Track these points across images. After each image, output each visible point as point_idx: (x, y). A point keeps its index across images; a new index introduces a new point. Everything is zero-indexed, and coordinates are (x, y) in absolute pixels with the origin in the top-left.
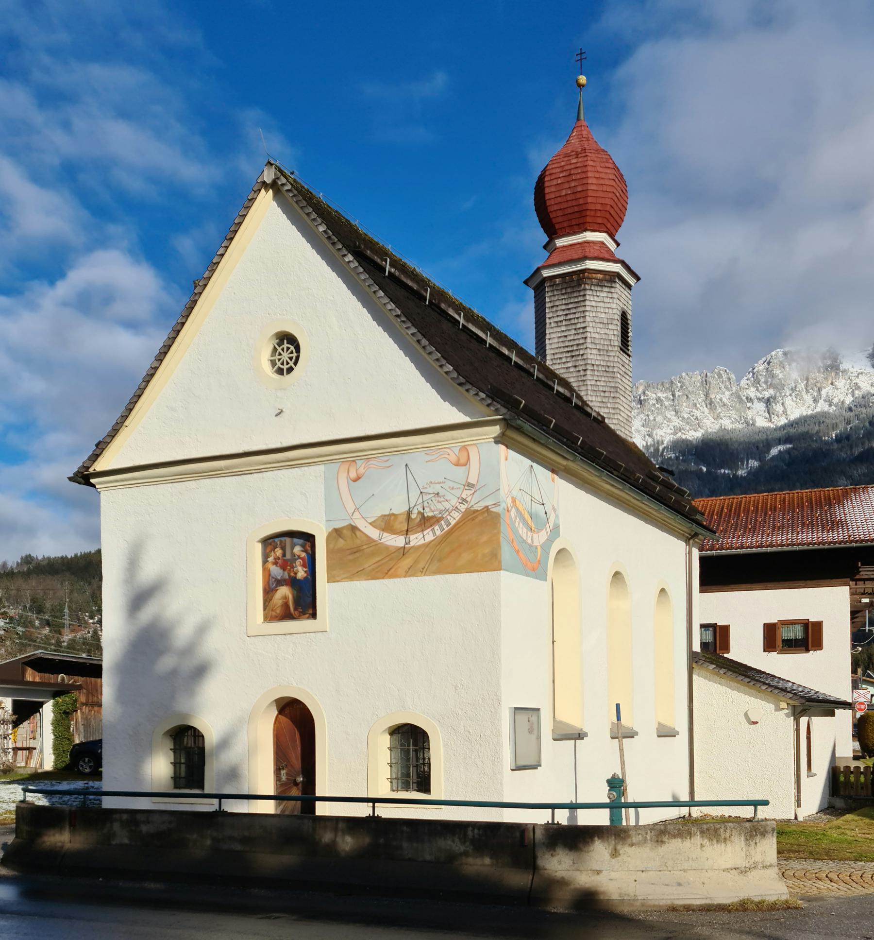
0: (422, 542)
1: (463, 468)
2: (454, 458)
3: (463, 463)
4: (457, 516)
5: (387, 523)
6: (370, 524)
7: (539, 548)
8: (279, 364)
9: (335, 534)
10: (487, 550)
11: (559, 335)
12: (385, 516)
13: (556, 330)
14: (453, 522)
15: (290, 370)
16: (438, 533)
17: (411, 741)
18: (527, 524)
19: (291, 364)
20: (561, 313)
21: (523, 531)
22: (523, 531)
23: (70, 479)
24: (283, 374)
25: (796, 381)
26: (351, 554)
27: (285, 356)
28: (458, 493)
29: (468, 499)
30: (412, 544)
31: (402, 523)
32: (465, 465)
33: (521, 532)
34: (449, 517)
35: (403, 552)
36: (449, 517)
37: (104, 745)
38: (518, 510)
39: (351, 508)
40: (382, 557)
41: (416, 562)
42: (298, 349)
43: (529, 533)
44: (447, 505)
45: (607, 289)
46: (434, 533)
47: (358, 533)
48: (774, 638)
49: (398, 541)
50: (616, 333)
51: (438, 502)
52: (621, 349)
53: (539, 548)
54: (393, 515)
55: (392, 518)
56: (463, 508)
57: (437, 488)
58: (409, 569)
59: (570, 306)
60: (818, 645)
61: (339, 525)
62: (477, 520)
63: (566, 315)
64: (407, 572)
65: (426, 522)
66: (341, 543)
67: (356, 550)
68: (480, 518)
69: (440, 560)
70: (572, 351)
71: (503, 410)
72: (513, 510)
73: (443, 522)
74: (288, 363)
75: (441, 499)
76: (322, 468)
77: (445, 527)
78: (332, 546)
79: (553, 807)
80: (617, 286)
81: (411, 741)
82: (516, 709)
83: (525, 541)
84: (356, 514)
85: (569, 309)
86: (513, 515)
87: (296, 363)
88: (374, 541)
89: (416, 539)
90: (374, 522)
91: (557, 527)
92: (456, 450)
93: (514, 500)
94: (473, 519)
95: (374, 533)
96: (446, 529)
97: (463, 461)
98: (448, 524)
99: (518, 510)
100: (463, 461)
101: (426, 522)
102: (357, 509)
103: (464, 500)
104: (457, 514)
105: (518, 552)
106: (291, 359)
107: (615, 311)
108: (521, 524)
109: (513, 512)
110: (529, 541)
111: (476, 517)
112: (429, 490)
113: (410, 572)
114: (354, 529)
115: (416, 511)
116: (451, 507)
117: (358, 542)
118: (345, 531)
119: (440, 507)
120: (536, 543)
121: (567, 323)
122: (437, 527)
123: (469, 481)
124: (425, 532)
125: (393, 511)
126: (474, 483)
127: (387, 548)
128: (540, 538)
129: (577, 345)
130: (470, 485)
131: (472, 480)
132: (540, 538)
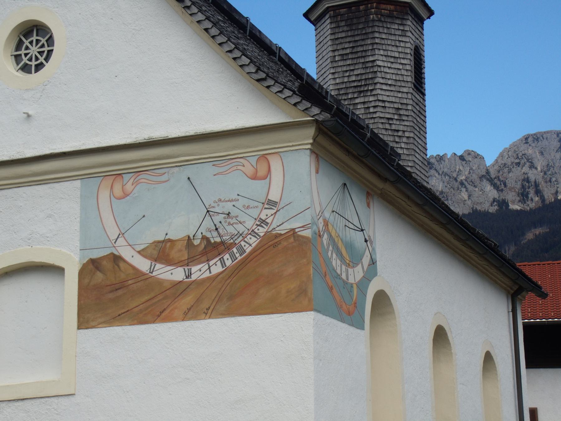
0: (207, 274)
1: (263, 181)
2: (249, 170)
3: (261, 175)
4: (254, 241)
5: (161, 252)
6: (139, 252)
7: (355, 286)
8: (25, 60)
9: (91, 266)
10: (293, 285)
11: (345, 69)
12: (159, 242)
13: (340, 64)
14: (248, 250)
15: (39, 67)
16: (228, 263)
18: (341, 255)
19: (42, 59)
20: (347, 46)
21: (336, 262)
22: (336, 262)
24: (30, 72)
25: (501, 184)
26: (111, 292)
27: (34, 50)
28: (255, 213)
29: (269, 221)
30: (194, 277)
31: (180, 251)
32: (264, 178)
33: (334, 263)
34: (243, 243)
35: (178, 289)
36: (243, 243)
37: (352, 329)
38: (330, 236)
39: (113, 233)
40: (152, 295)
41: (198, 301)
42: (50, 41)
43: (344, 267)
44: (241, 228)
45: (398, 21)
46: (223, 264)
47: (122, 265)
49: (177, 274)
50: (408, 67)
51: (229, 224)
52: (415, 86)
53: (355, 286)
54: (170, 240)
55: (168, 244)
56: (262, 231)
57: (228, 207)
58: (189, 310)
59: (357, 38)
61: (96, 254)
62: (280, 247)
63: (353, 47)
64: (186, 314)
66: (99, 277)
67: (121, 286)
68: (285, 243)
69: (231, 298)
70: (361, 86)
72: (326, 236)
73: (235, 250)
74: (37, 59)
75: (234, 221)
76: (78, 183)
77: (237, 255)
78: (86, 281)
80: (409, 23)
83: (339, 276)
84: (121, 241)
85: (355, 41)
86: (325, 242)
87: (47, 59)
88: (144, 274)
89: (199, 271)
90: (143, 250)
91: (373, 262)
92: (253, 160)
93: (326, 223)
94: (275, 245)
95: (143, 264)
96: (239, 258)
97: (262, 172)
98: (242, 251)
99: (330, 236)
100: (262, 172)
101: (212, 249)
102: (121, 234)
103: (263, 222)
104: (254, 239)
105: (331, 289)
106: (41, 53)
107: (408, 45)
108: (334, 256)
110: (344, 276)
111: (279, 243)
112: (217, 210)
113: (191, 314)
114: (116, 259)
115: (200, 236)
116: (246, 229)
117: (123, 276)
118: (104, 263)
119: (231, 229)
120: (351, 280)
121: (354, 56)
122: (227, 256)
123: (271, 197)
124: (211, 263)
125: (170, 236)
126: (277, 200)
127: (160, 282)
128: (356, 275)
129: (366, 79)
130: (272, 204)
131: (274, 196)
132: (356, 275)
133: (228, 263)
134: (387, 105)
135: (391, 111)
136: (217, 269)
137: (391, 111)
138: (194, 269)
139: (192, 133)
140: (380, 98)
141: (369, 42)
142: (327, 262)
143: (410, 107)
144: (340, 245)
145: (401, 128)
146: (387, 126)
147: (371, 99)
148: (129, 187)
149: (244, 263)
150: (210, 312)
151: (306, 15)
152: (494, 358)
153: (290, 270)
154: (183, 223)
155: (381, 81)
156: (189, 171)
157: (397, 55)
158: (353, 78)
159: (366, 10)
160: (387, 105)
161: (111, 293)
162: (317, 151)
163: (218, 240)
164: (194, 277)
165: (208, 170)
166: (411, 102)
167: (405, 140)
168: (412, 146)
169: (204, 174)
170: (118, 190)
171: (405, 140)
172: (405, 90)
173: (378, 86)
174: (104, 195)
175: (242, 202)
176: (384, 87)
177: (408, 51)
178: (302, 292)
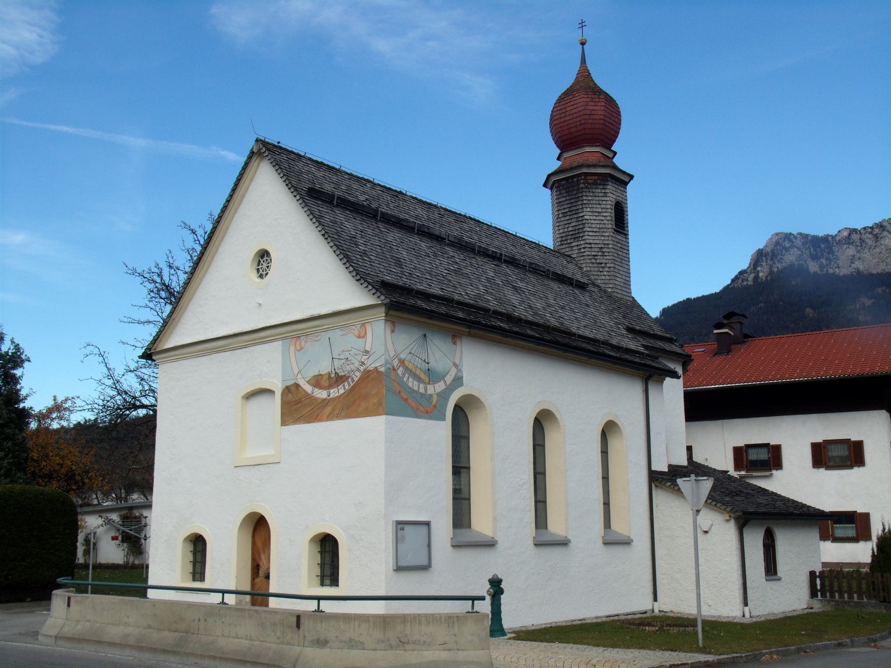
0: (337, 395)
2: (357, 332)
4: (358, 374)
5: (317, 381)
13: (563, 219)
14: (356, 379)
16: (347, 387)
17: (327, 546)
21: (412, 384)
23: (140, 357)
28: (359, 358)
30: (331, 396)
35: (325, 402)
39: (296, 371)
41: (333, 410)
45: (601, 187)
48: (824, 456)
50: (609, 218)
56: (362, 369)
57: (347, 355)
60: (778, 465)
61: (289, 383)
65: (339, 379)
67: (299, 401)
71: (383, 297)
76: (280, 342)
79: (223, 592)
80: (609, 187)
81: (327, 546)
82: (399, 523)
89: (335, 392)
93: (402, 362)
94: (368, 377)
95: (308, 388)
97: (362, 334)
99: (407, 369)
101: (339, 379)
109: (400, 371)
113: (331, 417)
114: (297, 386)
116: (354, 369)
119: (348, 368)
127: (316, 399)
130: (367, 352)
131: (368, 348)
133: (347, 387)
134: (593, 246)
135: (596, 250)
136: (342, 391)
137: (596, 250)
138: (332, 391)
139: (327, 313)
140: (588, 241)
141: (580, 203)
142: (404, 386)
143: (610, 246)
144: (418, 372)
145: (604, 261)
146: (594, 261)
147: (582, 242)
148: (303, 344)
149: (354, 387)
150: (339, 417)
151: (545, 185)
152: (619, 424)
153: (375, 392)
154: (324, 367)
155: (589, 229)
156: (330, 334)
157: (600, 210)
158: (570, 229)
159: (578, 181)
160: (593, 246)
161: (297, 407)
162: (389, 318)
163: (343, 374)
164: (331, 396)
165: (338, 333)
166: (611, 242)
167: (607, 269)
168: (612, 273)
169: (336, 335)
170: (298, 347)
171: (607, 269)
172: (607, 234)
173: (586, 233)
174: (292, 348)
175: (354, 351)
176: (591, 234)
177: (609, 207)
178: (380, 404)
